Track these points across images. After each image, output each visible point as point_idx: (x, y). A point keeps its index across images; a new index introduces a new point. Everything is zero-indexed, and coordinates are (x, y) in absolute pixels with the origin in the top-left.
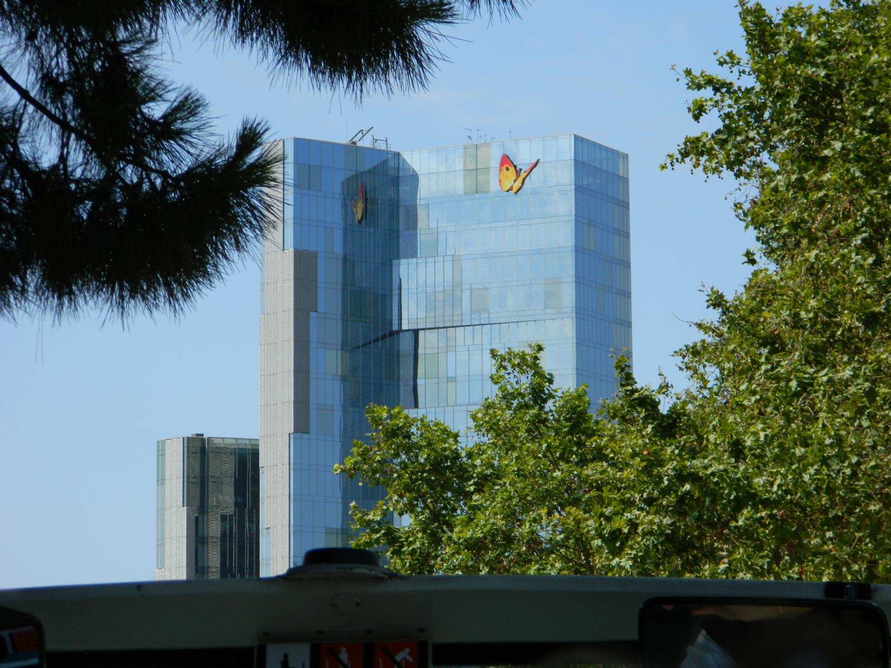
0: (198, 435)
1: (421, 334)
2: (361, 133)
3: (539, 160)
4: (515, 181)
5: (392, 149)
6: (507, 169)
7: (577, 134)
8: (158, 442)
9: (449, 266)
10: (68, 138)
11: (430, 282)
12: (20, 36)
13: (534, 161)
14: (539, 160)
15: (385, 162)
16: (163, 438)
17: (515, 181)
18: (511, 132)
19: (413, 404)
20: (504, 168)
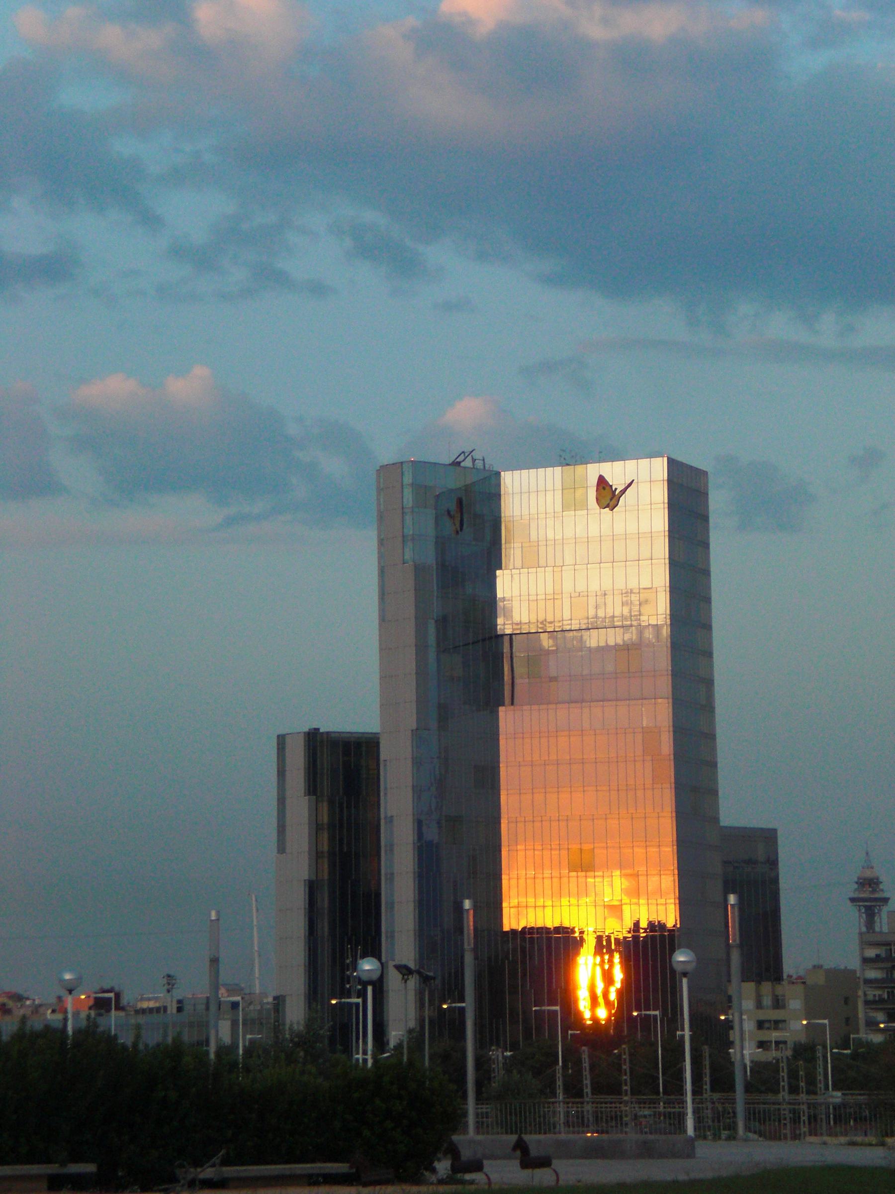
0: (315, 729)
1: (514, 636)
2: (463, 455)
3: (633, 480)
4: (611, 500)
5: (495, 469)
6: (604, 488)
7: (673, 457)
8: (278, 736)
9: (549, 576)
10: (611, 961)
11: (533, 591)
12: (386, 813)
13: (628, 482)
14: (633, 480)
15: (489, 477)
16: (284, 733)
17: (611, 500)
18: (600, 452)
19: (510, 703)
20: (601, 488)
